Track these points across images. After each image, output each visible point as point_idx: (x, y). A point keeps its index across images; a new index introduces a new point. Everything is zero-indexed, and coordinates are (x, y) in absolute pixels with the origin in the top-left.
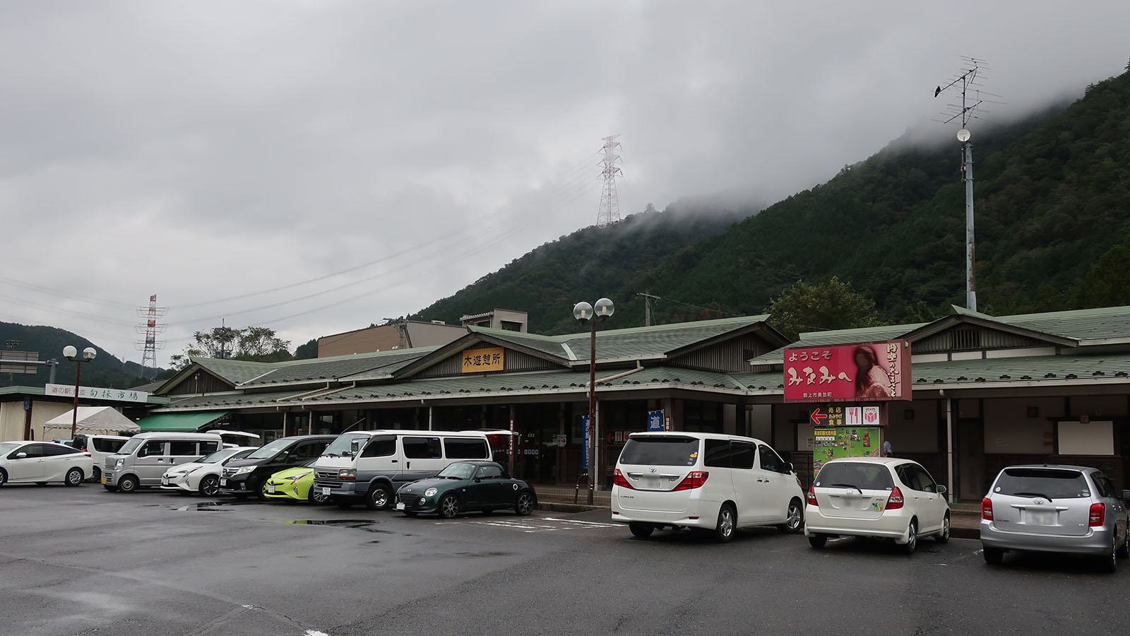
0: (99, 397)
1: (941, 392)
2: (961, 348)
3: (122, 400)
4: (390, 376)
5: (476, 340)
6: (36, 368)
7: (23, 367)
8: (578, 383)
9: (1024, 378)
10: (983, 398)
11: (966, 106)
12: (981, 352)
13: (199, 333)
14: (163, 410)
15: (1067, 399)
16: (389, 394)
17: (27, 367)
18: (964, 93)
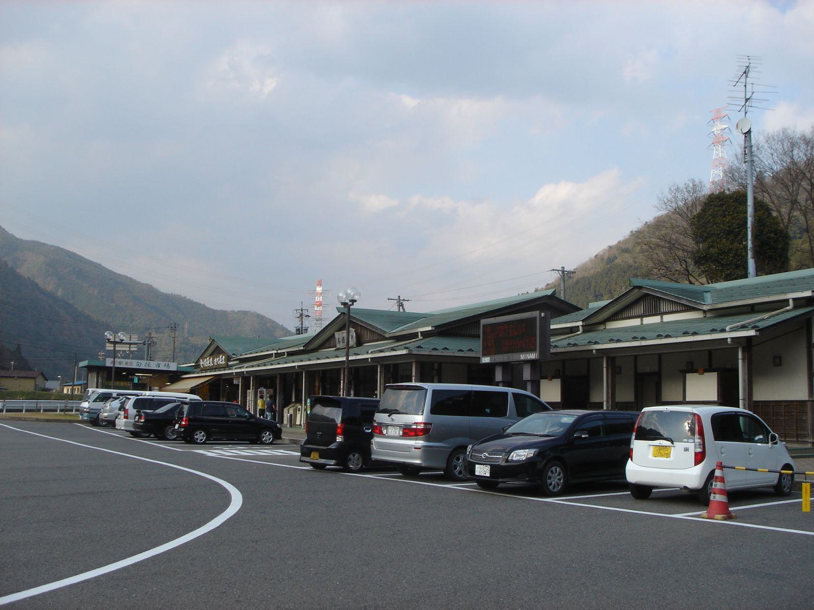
0: (143, 367)
1: (729, 340)
2: (658, 313)
3: (159, 369)
4: (302, 348)
5: (636, 294)
6: (136, 346)
7: (128, 346)
8: (691, 331)
9: (470, 350)
10: (615, 357)
11: (747, 98)
12: (660, 316)
13: (353, 301)
14: (191, 376)
15: (710, 352)
16: (590, 342)
17: (131, 346)
18: (745, 86)
